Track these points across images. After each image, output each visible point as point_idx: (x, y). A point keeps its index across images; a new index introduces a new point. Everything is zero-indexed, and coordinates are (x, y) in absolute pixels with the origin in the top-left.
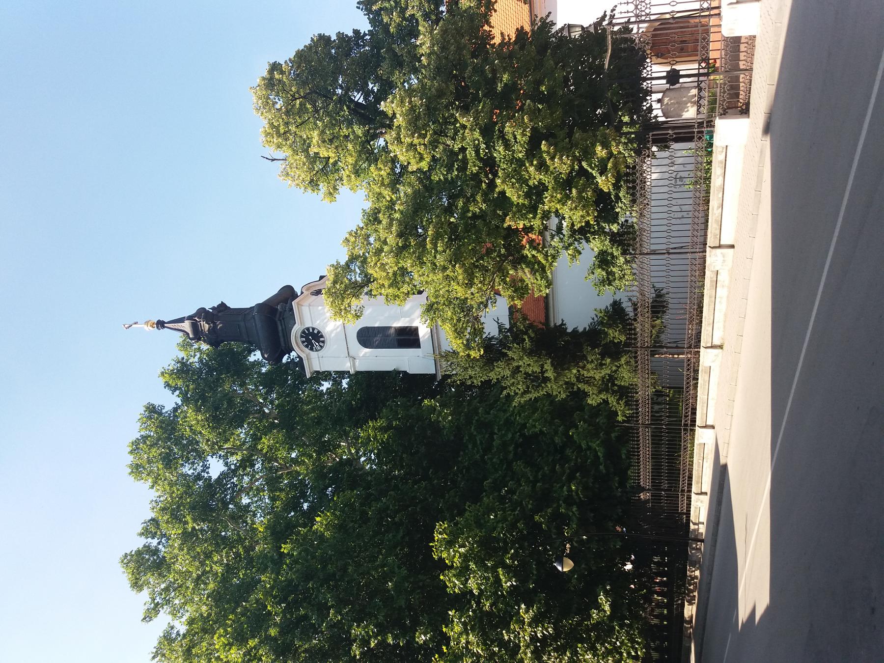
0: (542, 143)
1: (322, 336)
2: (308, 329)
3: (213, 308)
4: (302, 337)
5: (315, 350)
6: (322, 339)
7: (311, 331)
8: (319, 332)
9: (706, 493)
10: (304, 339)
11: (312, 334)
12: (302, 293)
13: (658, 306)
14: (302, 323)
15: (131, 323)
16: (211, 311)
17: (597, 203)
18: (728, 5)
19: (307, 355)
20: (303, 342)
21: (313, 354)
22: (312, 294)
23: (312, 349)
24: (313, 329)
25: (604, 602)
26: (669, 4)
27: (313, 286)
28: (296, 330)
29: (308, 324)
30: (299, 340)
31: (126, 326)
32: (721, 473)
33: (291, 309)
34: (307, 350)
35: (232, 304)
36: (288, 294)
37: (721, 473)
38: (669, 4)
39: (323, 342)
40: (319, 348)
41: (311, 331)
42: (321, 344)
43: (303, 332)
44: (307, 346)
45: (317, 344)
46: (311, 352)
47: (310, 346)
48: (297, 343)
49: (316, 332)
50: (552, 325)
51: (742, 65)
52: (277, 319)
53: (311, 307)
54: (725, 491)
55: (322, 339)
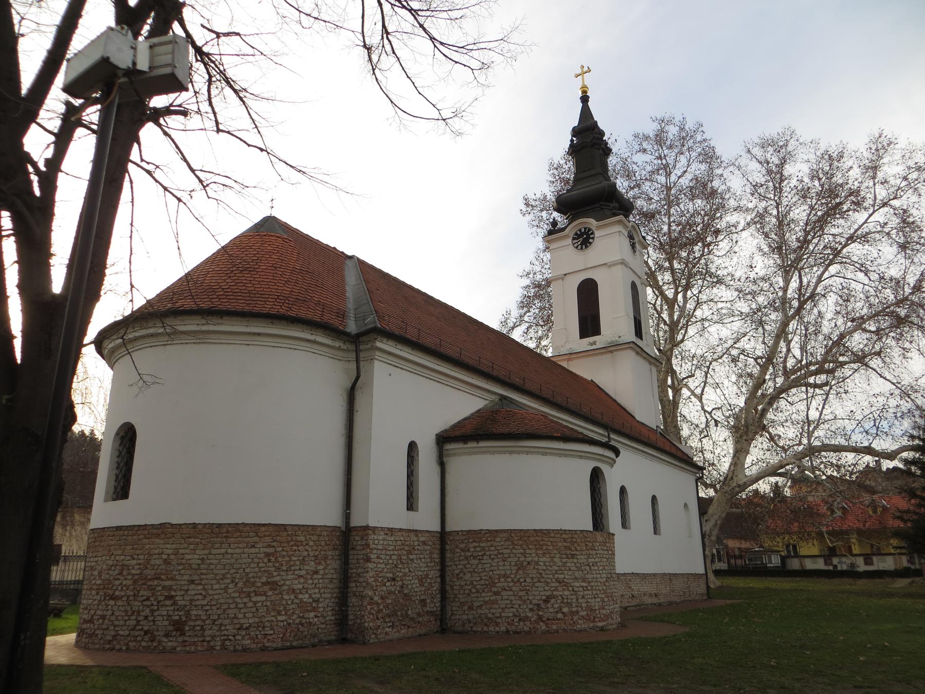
0: (150, 14)
1: (586, 247)
2: (593, 233)
4: (585, 229)
6: (584, 247)
7: (591, 236)
8: (590, 243)
10: (583, 230)
11: (588, 237)
13: (846, 392)
14: (599, 228)
18: (654, 498)
19: (567, 235)
21: (569, 241)
23: (574, 239)
24: (593, 238)
26: (472, 69)
27: (637, 233)
28: (592, 222)
29: (597, 234)
32: (623, 491)
33: (615, 215)
34: (572, 235)
37: (623, 491)
38: (472, 69)
40: (576, 245)
41: (591, 236)
42: (580, 247)
43: (590, 230)
44: (576, 234)
45: (579, 243)
47: (577, 236)
49: (591, 240)
52: (601, 203)
55: (584, 247)
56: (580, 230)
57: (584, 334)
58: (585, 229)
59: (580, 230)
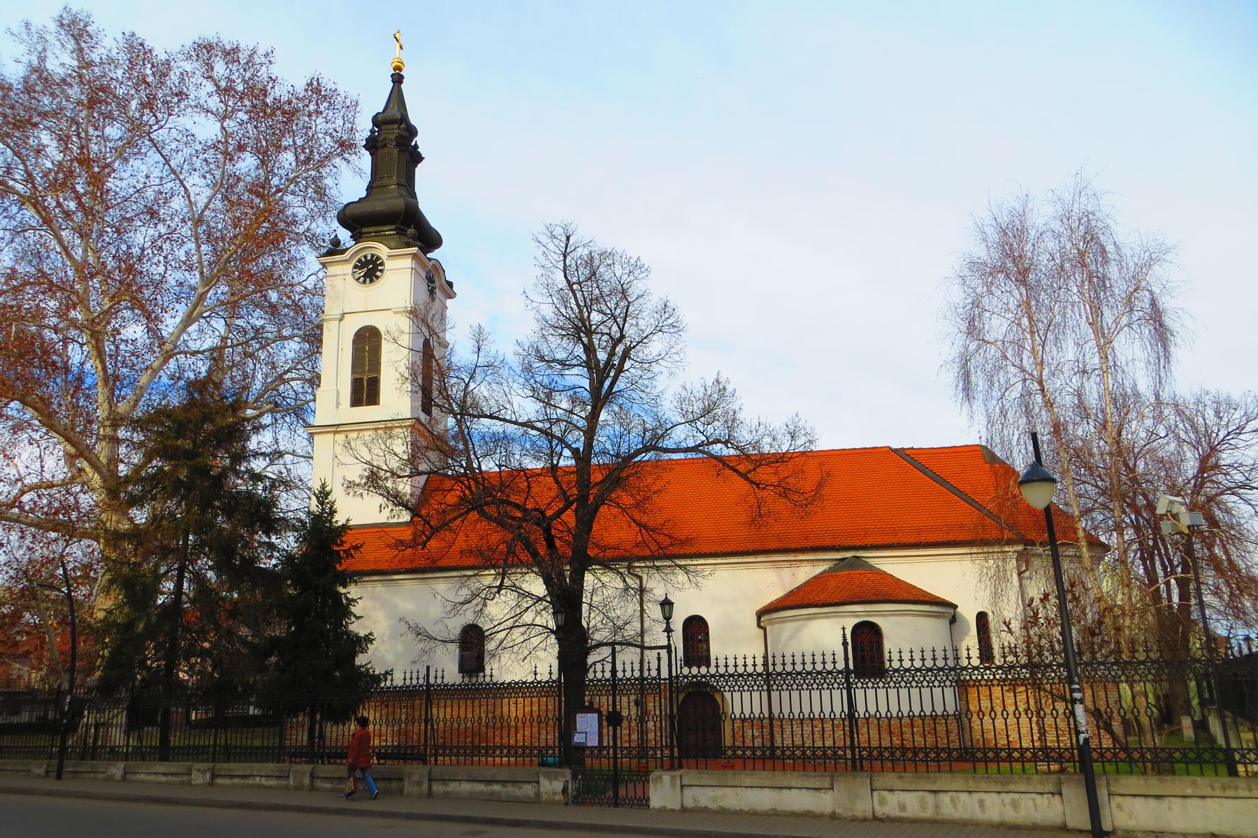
1: (371, 281)
2: (382, 264)
3: (416, 146)
4: (372, 256)
6: (368, 280)
8: (377, 277)
9: (659, 654)
10: (369, 258)
11: (375, 269)
12: (430, 259)
15: (401, 41)
16: (413, 144)
17: (259, 474)
20: (365, 257)
21: (348, 268)
22: (428, 272)
23: (355, 267)
24: (381, 271)
25: (1181, 426)
28: (382, 250)
29: (389, 265)
30: (369, 253)
31: (398, 36)
34: (354, 261)
35: (420, 170)
36: (428, 239)
39: (364, 282)
40: (357, 276)
42: (362, 279)
43: (378, 258)
44: (359, 261)
46: (351, 266)
49: (378, 273)
50: (352, 591)
51: (332, 761)
53: (646, 645)
54: (921, 459)
55: (368, 280)
57: (356, 401)
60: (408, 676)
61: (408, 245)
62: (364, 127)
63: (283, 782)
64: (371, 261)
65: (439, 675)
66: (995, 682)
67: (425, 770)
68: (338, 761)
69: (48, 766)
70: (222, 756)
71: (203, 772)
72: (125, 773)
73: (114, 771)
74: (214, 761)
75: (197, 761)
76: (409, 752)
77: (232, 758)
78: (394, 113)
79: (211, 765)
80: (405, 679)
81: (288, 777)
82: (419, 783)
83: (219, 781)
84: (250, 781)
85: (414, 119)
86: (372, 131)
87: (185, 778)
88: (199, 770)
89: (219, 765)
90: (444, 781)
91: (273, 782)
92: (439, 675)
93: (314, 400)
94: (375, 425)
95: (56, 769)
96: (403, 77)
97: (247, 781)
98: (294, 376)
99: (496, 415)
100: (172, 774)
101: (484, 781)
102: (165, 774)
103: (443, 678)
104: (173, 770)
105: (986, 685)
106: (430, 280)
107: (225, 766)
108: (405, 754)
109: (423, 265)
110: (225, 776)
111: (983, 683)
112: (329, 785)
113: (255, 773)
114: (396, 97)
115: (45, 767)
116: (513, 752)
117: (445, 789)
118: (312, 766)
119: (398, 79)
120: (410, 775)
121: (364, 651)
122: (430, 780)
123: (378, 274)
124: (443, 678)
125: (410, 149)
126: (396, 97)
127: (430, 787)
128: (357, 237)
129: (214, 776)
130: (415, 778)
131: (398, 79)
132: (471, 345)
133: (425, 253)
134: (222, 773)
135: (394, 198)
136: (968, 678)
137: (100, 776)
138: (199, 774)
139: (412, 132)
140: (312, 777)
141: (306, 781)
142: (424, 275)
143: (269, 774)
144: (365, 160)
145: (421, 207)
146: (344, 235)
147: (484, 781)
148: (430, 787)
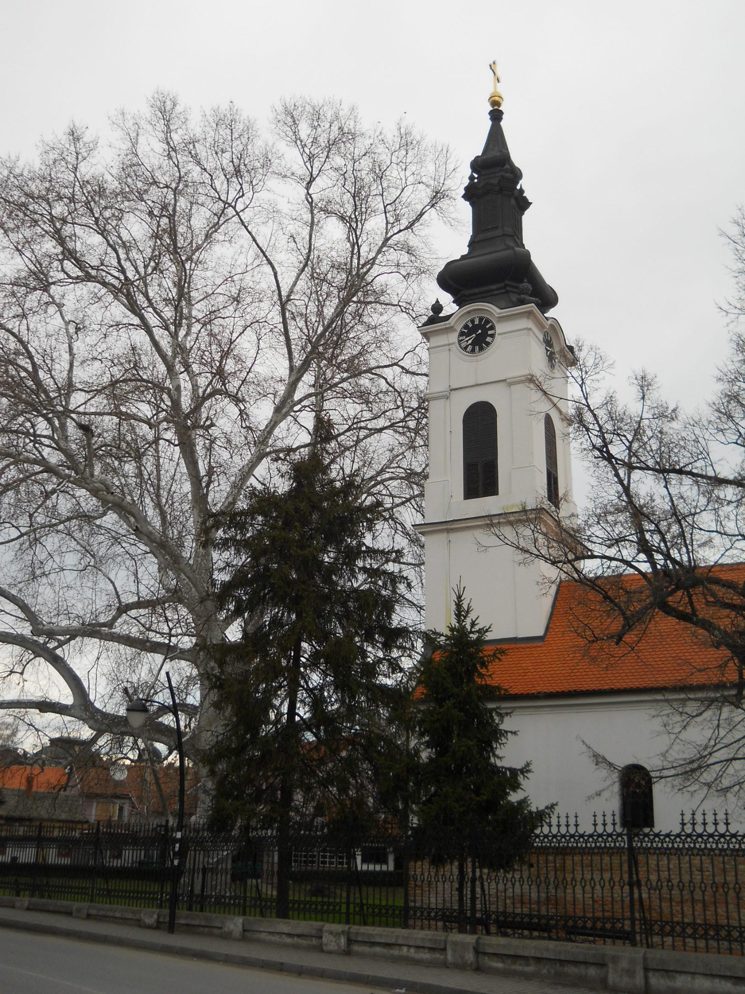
1: (481, 349)
2: (493, 328)
3: (522, 191)
5: (461, 338)
6: (477, 348)
7: (490, 332)
8: (488, 344)
10: (477, 322)
11: (485, 334)
14: (502, 319)
16: (518, 187)
19: (452, 327)
21: (454, 337)
22: (546, 334)
23: (462, 334)
24: (492, 336)
28: (493, 310)
29: (500, 328)
34: (459, 327)
35: (528, 219)
39: (473, 351)
40: (464, 345)
41: (490, 332)
42: (470, 348)
43: (488, 321)
44: (466, 327)
45: (470, 342)
46: (457, 334)
48: (469, 312)
55: (477, 348)
56: (472, 321)
58: (481, 319)
59: (472, 321)
60: (600, 820)
61: (522, 302)
62: (462, 176)
63: (437, 956)
64: (479, 326)
65: (572, 821)
66: (652, 851)
67: (639, 952)
68: (526, 932)
69: (159, 916)
70: (357, 917)
71: (337, 935)
72: (244, 931)
73: (232, 927)
74: (348, 922)
75: (328, 921)
76: (608, 926)
77: (370, 920)
78: (495, 153)
79: (346, 927)
80: (595, 825)
81: (444, 949)
82: (631, 973)
83: (356, 948)
84: (395, 952)
85: (517, 158)
86: (471, 178)
87: (315, 942)
88: (331, 933)
89: (355, 928)
90: (667, 972)
91: (425, 956)
92: (572, 821)
93: (422, 495)
94: (490, 522)
95: (167, 919)
96: (501, 113)
97: (392, 952)
98: (387, 476)
99: (688, 469)
100: (299, 936)
101: (731, 977)
102: (290, 935)
103: (577, 825)
104: (299, 931)
105: (709, 855)
106: (548, 343)
107: (363, 929)
108: (594, 928)
109: (540, 326)
110: (364, 943)
111: (706, 852)
112: (500, 965)
113: (400, 941)
114: (496, 137)
115: (155, 916)
116: (723, 933)
117: (671, 984)
118: (475, 937)
119: (496, 115)
120: (615, 959)
121: (516, 786)
122: (646, 970)
123: (489, 339)
124: (577, 825)
125: (516, 193)
126: (496, 137)
127: (646, 978)
128: (460, 301)
129: (350, 942)
130: (624, 964)
131: (496, 115)
132: (634, 391)
133: (543, 313)
134: (360, 939)
135: (502, 250)
136: (584, 845)
137: (216, 931)
138: (331, 938)
139: (516, 175)
140: (477, 952)
141: (470, 957)
142: (541, 337)
143: (419, 943)
144: (465, 211)
145: (532, 258)
146: (446, 300)
147: (731, 977)
148: (646, 978)
